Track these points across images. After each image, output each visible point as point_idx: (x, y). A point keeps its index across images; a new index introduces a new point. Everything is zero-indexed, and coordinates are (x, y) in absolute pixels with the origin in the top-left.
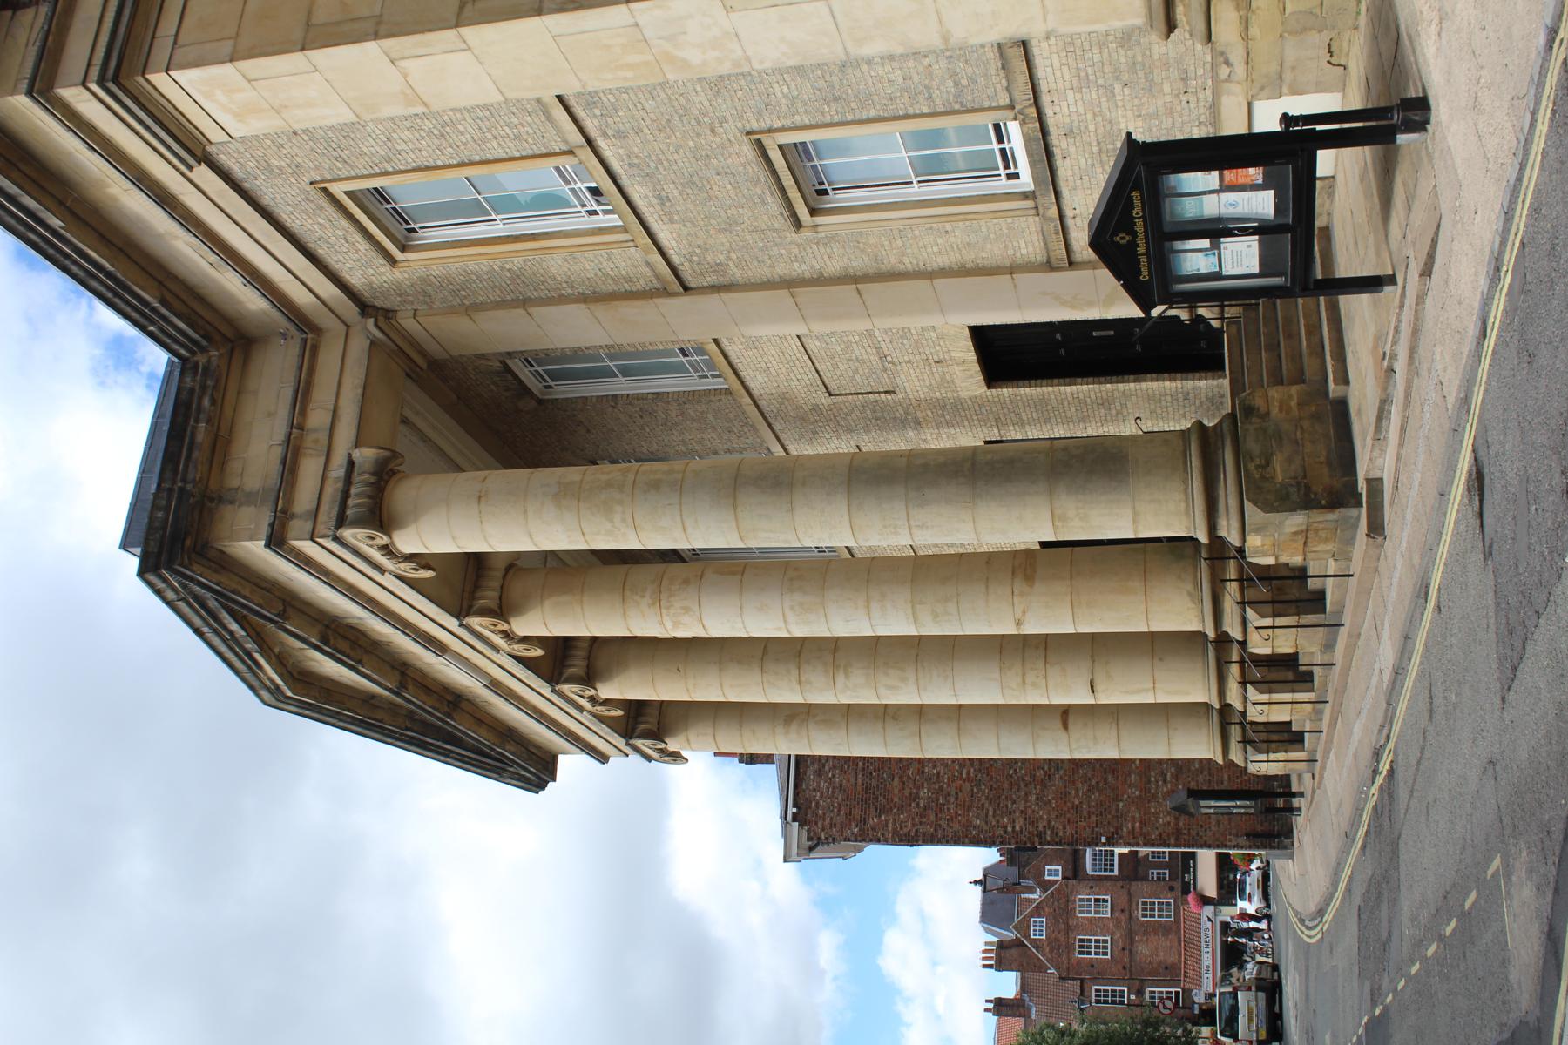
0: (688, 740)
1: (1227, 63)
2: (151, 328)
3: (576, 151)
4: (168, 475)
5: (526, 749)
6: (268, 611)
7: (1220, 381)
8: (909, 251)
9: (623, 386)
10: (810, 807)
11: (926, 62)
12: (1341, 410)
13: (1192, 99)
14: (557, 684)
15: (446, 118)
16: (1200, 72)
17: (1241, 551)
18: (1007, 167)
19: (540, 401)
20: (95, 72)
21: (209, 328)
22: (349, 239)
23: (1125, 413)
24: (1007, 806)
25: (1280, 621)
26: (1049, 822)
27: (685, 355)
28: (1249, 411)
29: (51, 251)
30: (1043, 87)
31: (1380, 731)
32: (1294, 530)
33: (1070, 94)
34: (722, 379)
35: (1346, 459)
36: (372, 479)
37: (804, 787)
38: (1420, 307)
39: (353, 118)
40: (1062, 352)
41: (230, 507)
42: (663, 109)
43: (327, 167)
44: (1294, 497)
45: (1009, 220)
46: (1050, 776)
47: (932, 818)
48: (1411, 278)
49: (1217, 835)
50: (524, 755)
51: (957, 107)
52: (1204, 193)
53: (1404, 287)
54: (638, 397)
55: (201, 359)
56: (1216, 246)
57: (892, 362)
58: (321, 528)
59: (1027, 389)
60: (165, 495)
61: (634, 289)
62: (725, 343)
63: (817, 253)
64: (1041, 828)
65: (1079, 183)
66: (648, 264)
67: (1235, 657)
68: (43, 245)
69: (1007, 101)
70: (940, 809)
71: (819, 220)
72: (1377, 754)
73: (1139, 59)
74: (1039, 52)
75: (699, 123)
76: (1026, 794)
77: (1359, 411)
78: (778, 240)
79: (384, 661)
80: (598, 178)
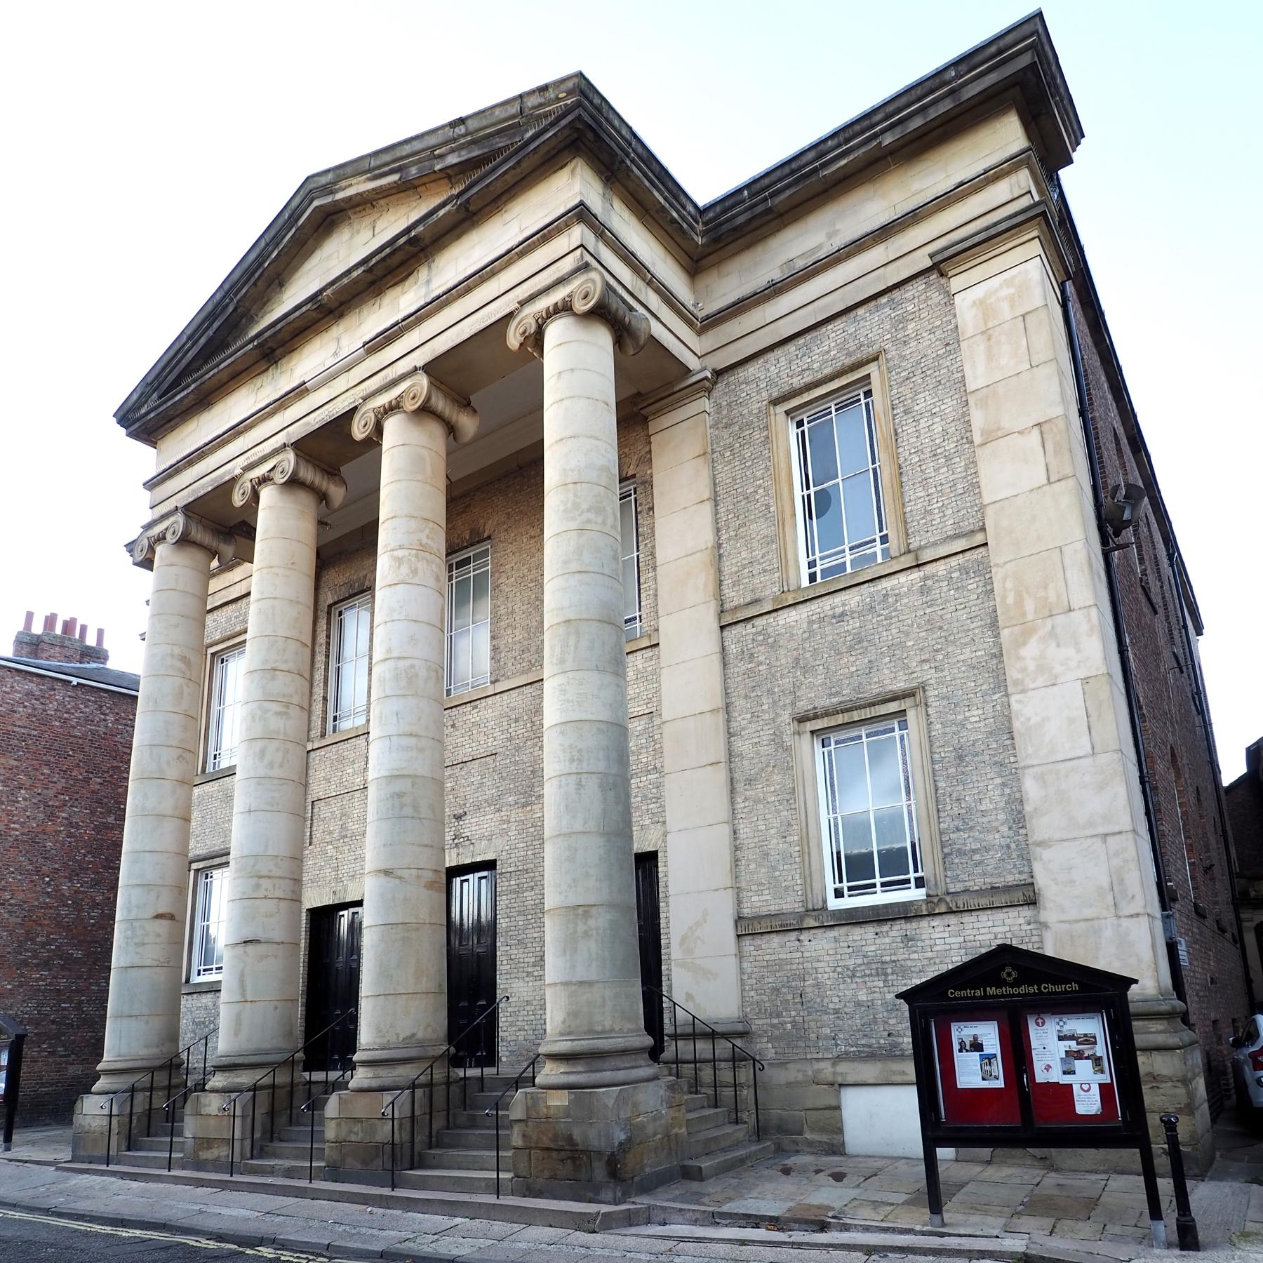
5: (177, 416)
6: (477, 193)
23: (527, 979)
43: (902, 364)
50: (172, 412)
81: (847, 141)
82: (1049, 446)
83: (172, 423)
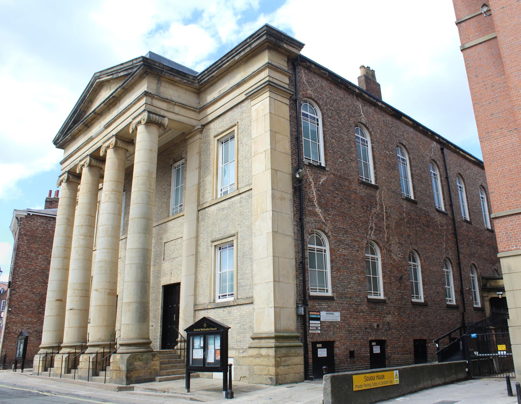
0: (65, 189)
1: (243, 352)
2: (206, 72)
3: (238, 190)
4: (168, 68)
7: (159, 348)
8: (203, 269)
9: (173, 188)
10: (32, 219)
11: (250, 279)
12: (152, 380)
13: (235, 343)
14: (90, 156)
15: (250, 160)
16: (242, 345)
17: (83, 353)
18: (222, 296)
19: (172, 165)
20: (271, 80)
21: (204, 85)
22: (222, 127)
24: (25, 279)
25: (91, 363)
26: (18, 292)
27: (180, 206)
28: (154, 356)
29: (230, 54)
30: (241, 307)
31: (57, 392)
32: (121, 367)
33: (239, 313)
34: (172, 215)
35: (140, 381)
36: (159, 122)
37: (39, 218)
38: (182, 398)
39: (253, 137)
40: (170, 306)
41: (157, 82)
42: (246, 214)
44: (130, 367)
45: (208, 296)
46: (33, 293)
47: (24, 256)
48: (189, 396)
49: (7, 345)
51: (238, 285)
52: (215, 345)
53: (187, 394)
54: (170, 192)
55: (196, 82)
56: (201, 348)
57: (172, 261)
58: (148, 106)
59: (161, 296)
60: (163, 67)
61: (200, 197)
62: (183, 217)
63: (204, 245)
64: (16, 290)
65: (217, 314)
66: (207, 202)
67: (77, 351)
68: (231, 53)
69: (239, 298)
70: (27, 259)
71: (213, 247)
72: (48, 392)
73: (246, 331)
74: (250, 306)
75: (241, 221)
76: (28, 286)
77: (152, 384)
78: (209, 236)
79: (104, 110)
80: (230, 194)
81: (228, 58)
82: (266, 158)
83: (67, 144)
